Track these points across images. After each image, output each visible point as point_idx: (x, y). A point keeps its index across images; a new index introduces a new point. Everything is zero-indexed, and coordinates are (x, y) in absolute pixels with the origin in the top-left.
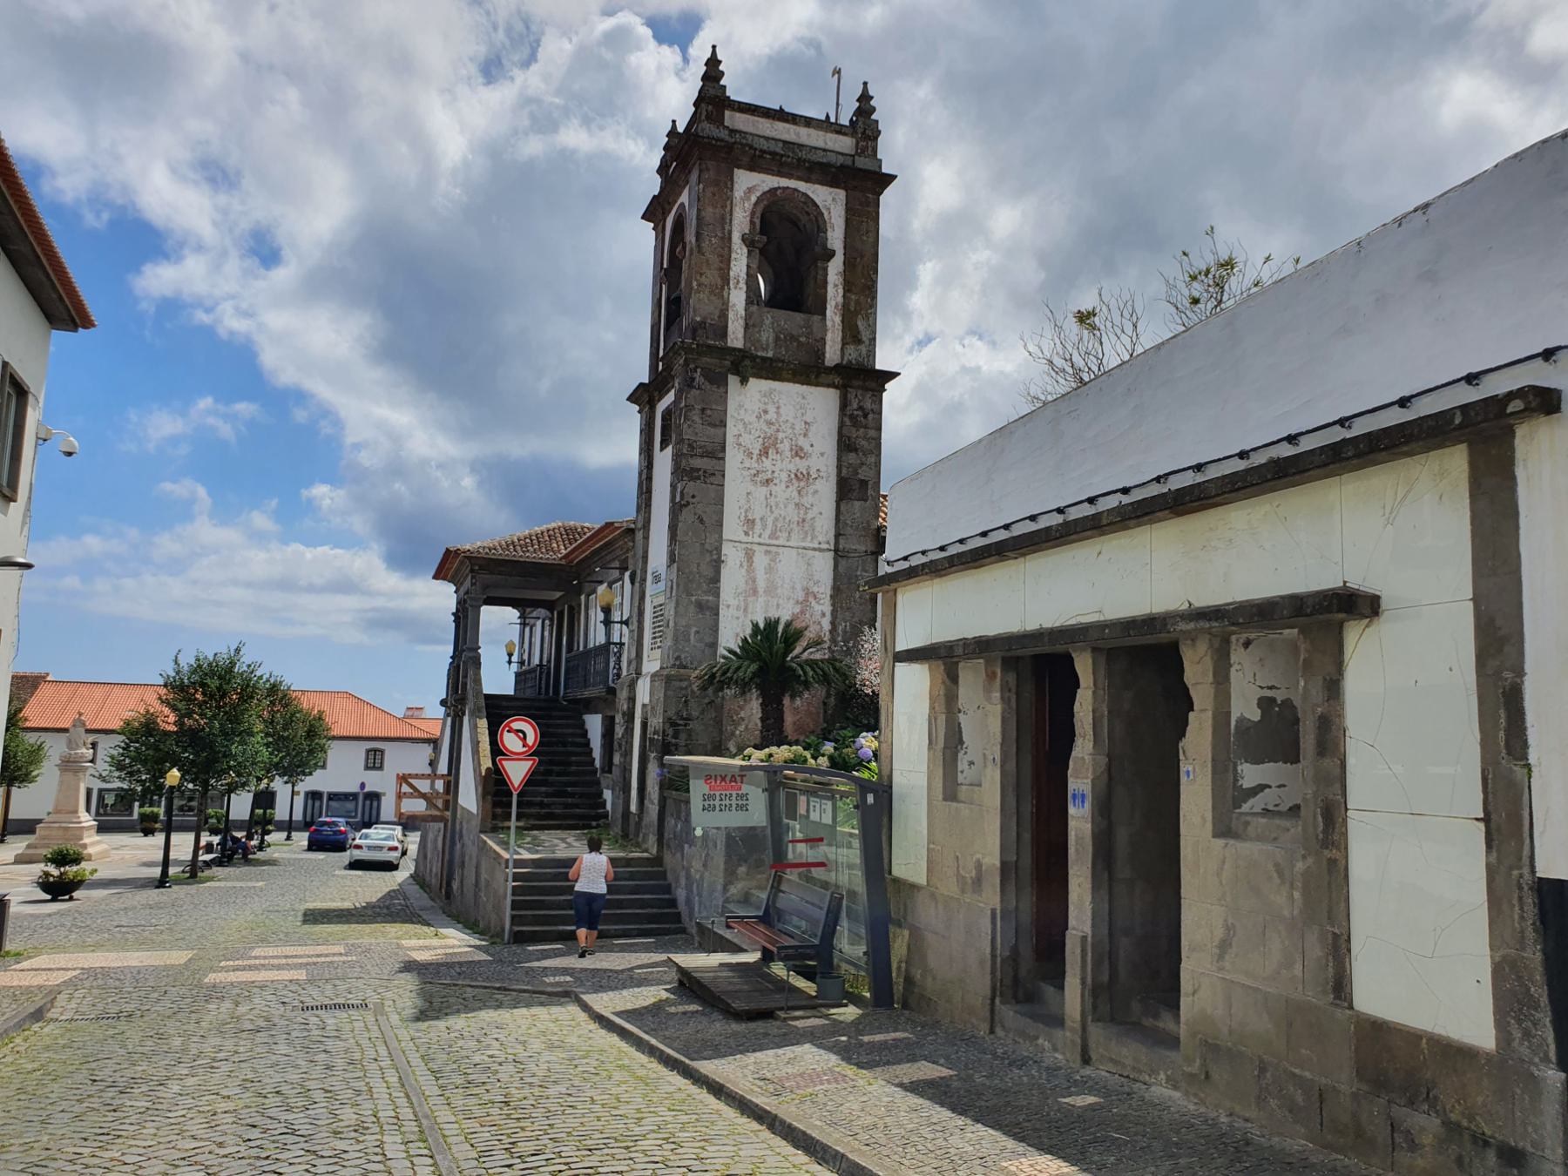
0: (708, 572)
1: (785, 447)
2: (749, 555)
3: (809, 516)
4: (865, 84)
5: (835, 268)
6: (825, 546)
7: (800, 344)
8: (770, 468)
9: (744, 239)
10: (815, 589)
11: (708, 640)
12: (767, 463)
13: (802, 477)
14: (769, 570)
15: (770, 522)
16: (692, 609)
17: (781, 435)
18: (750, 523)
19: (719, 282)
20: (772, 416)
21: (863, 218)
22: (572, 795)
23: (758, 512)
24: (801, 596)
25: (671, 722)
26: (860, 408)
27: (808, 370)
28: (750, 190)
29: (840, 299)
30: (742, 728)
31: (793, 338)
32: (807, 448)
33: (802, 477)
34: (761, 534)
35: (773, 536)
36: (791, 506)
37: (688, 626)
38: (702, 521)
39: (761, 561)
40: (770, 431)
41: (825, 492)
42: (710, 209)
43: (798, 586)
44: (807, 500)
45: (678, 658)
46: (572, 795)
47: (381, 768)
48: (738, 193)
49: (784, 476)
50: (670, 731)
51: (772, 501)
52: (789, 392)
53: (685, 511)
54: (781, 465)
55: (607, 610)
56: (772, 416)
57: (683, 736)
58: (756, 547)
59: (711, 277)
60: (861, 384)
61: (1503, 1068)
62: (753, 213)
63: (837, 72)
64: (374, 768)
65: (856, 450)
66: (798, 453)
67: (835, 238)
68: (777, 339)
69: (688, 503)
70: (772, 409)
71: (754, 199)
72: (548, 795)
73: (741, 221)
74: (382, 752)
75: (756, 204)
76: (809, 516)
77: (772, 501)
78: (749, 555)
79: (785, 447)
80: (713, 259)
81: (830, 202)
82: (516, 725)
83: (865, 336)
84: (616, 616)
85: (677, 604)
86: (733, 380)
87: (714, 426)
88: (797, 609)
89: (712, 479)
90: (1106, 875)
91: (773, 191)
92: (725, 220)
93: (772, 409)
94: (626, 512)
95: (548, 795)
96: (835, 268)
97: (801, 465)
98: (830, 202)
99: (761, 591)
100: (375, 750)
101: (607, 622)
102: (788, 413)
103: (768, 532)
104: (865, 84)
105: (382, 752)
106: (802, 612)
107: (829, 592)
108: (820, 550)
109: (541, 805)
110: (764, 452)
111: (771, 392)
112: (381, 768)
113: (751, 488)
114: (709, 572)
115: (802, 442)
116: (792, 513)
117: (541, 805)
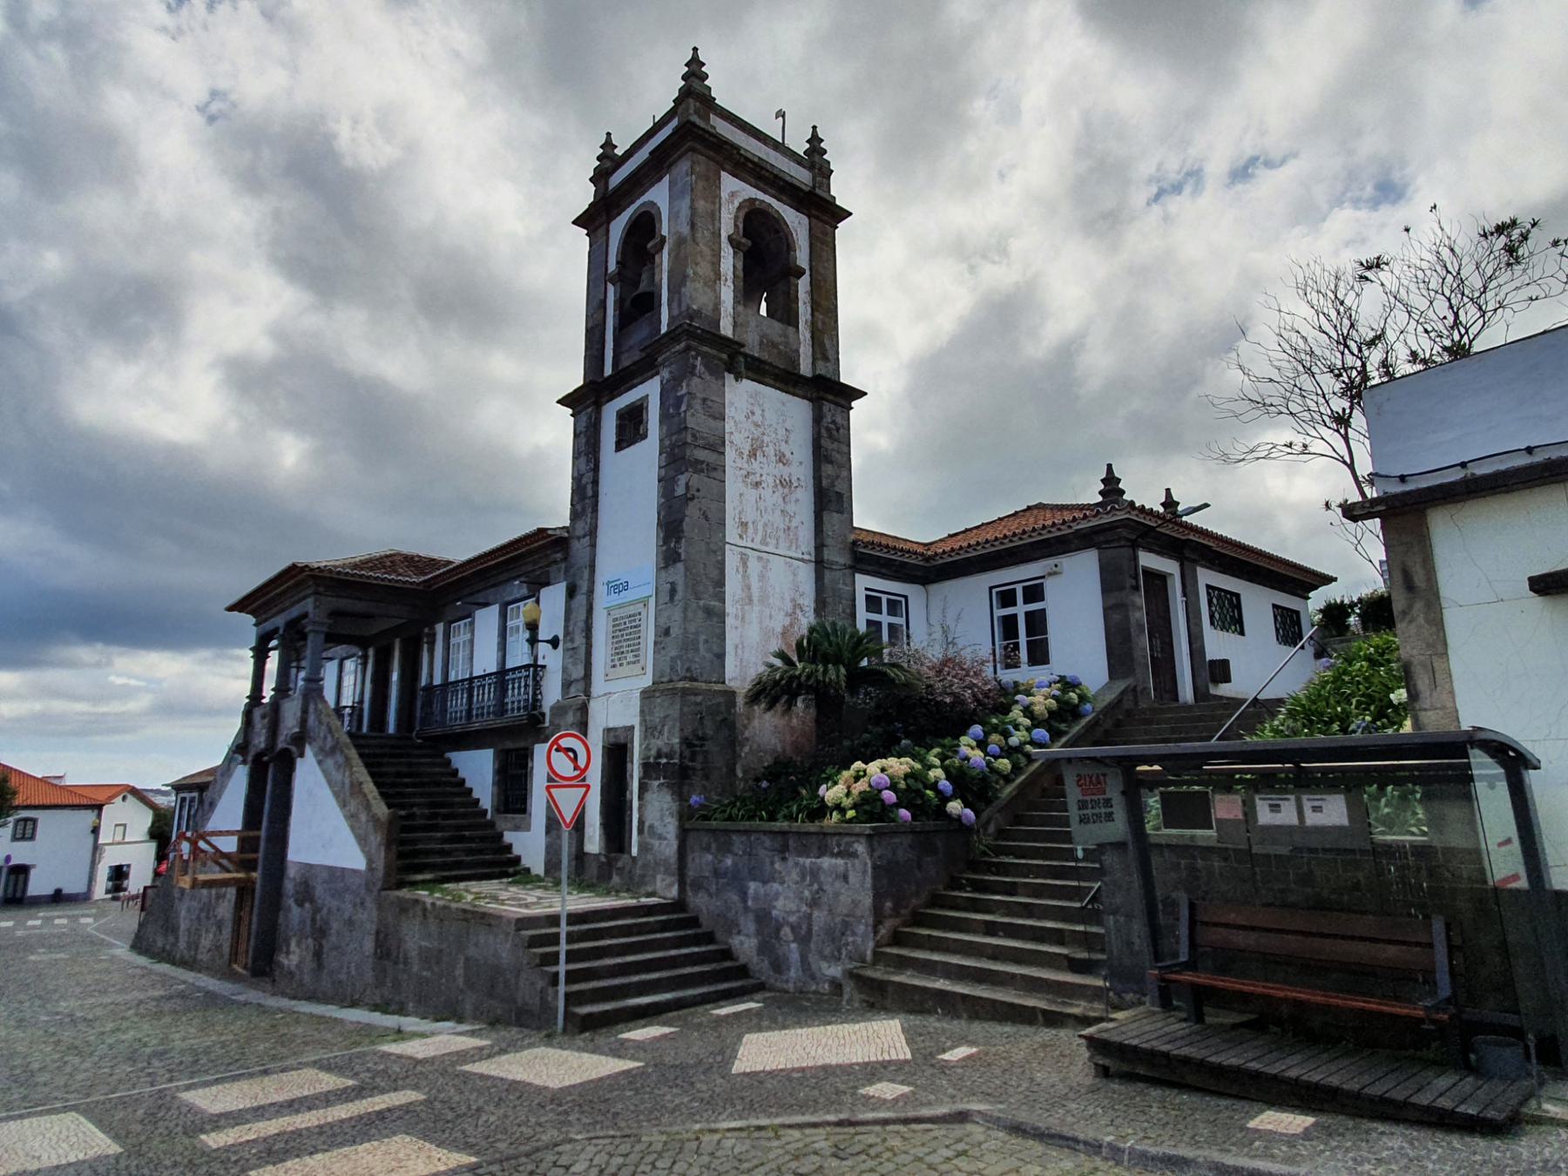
0: (714, 574)
1: (770, 450)
2: (744, 560)
3: (793, 524)
4: (814, 128)
5: (803, 284)
6: (806, 557)
7: (780, 352)
8: (759, 471)
9: (730, 238)
10: (801, 601)
11: (716, 649)
12: (756, 465)
13: (785, 483)
14: (762, 577)
15: (760, 528)
16: (700, 614)
17: (766, 439)
18: (744, 525)
19: (712, 275)
20: (757, 418)
21: (824, 249)
22: (471, 839)
23: (749, 516)
24: (789, 607)
25: (686, 742)
26: (834, 422)
27: (785, 378)
28: (733, 194)
29: (809, 317)
30: (747, 749)
31: (774, 345)
32: (788, 454)
33: (785, 483)
34: (754, 539)
35: (764, 542)
36: (778, 512)
37: (697, 633)
38: (707, 519)
39: (754, 566)
40: (757, 433)
41: (804, 500)
42: (702, 203)
43: (788, 598)
44: (791, 508)
45: (688, 670)
46: (471, 839)
47: (32, 838)
48: (724, 195)
49: (770, 480)
50: (687, 753)
51: (762, 505)
52: (771, 397)
53: (691, 504)
54: (767, 469)
55: (533, 627)
56: (757, 418)
57: (700, 758)
58: (749, 552)
59: (704, 269)
60: (830, 396)
61: (726, 1075)
62: (736, 218)
63: (781, 114)
64: (23, 838)
65: (831, 462)
66: (781, 459)
67: (802, 258)
68: (761, 343)
69: (692, 498)
70: (758, 412)
71: (737, 204)
72: (445, 840)
73: (727, 226)
74: (34, 821)
75: (739, 208)
76: (793, 524)
77: (762, 505)
78: (744, 560)
79: (770, 450)
80: (706, 251)
81: (796, 222)
82: (565, 743)
83: (830, 354)
84: (544, 633)
85: (685, 610)
86: (729, 378)
87: (715, 418)
88: (787, 622)
89: (714, 474)
90: (825, 483)
91: (752, 201)
92: (714, 216)
93: (758, 412)
94: (557, 514)
95: (445, 840)
96: (803, 284)
97: (785, 471)
98: (796, 222)
99: (755, 599)
100: (26, 820)
101: (533, 641)
102: (771, 417)
103: (758, 538)
104: (814, 128)
105: (34, 821)
106: (791, 625)
107: (813, 605)
108: (802, 560)
109: (442, 853)
110: (753, 454)
111: (757, 393)
112: (32, 838)
113: (744, 490)
114: (714, 574)
115: (784, 448)
116: (777, 520)
117: (442, 853)
